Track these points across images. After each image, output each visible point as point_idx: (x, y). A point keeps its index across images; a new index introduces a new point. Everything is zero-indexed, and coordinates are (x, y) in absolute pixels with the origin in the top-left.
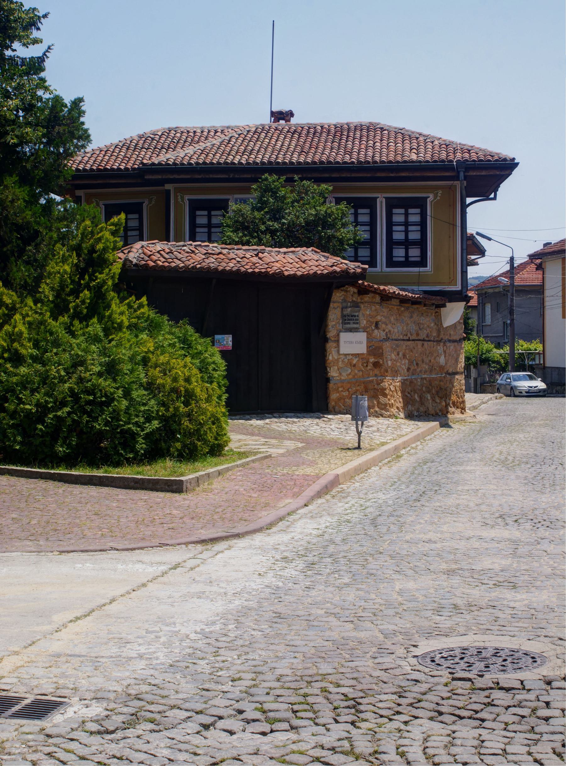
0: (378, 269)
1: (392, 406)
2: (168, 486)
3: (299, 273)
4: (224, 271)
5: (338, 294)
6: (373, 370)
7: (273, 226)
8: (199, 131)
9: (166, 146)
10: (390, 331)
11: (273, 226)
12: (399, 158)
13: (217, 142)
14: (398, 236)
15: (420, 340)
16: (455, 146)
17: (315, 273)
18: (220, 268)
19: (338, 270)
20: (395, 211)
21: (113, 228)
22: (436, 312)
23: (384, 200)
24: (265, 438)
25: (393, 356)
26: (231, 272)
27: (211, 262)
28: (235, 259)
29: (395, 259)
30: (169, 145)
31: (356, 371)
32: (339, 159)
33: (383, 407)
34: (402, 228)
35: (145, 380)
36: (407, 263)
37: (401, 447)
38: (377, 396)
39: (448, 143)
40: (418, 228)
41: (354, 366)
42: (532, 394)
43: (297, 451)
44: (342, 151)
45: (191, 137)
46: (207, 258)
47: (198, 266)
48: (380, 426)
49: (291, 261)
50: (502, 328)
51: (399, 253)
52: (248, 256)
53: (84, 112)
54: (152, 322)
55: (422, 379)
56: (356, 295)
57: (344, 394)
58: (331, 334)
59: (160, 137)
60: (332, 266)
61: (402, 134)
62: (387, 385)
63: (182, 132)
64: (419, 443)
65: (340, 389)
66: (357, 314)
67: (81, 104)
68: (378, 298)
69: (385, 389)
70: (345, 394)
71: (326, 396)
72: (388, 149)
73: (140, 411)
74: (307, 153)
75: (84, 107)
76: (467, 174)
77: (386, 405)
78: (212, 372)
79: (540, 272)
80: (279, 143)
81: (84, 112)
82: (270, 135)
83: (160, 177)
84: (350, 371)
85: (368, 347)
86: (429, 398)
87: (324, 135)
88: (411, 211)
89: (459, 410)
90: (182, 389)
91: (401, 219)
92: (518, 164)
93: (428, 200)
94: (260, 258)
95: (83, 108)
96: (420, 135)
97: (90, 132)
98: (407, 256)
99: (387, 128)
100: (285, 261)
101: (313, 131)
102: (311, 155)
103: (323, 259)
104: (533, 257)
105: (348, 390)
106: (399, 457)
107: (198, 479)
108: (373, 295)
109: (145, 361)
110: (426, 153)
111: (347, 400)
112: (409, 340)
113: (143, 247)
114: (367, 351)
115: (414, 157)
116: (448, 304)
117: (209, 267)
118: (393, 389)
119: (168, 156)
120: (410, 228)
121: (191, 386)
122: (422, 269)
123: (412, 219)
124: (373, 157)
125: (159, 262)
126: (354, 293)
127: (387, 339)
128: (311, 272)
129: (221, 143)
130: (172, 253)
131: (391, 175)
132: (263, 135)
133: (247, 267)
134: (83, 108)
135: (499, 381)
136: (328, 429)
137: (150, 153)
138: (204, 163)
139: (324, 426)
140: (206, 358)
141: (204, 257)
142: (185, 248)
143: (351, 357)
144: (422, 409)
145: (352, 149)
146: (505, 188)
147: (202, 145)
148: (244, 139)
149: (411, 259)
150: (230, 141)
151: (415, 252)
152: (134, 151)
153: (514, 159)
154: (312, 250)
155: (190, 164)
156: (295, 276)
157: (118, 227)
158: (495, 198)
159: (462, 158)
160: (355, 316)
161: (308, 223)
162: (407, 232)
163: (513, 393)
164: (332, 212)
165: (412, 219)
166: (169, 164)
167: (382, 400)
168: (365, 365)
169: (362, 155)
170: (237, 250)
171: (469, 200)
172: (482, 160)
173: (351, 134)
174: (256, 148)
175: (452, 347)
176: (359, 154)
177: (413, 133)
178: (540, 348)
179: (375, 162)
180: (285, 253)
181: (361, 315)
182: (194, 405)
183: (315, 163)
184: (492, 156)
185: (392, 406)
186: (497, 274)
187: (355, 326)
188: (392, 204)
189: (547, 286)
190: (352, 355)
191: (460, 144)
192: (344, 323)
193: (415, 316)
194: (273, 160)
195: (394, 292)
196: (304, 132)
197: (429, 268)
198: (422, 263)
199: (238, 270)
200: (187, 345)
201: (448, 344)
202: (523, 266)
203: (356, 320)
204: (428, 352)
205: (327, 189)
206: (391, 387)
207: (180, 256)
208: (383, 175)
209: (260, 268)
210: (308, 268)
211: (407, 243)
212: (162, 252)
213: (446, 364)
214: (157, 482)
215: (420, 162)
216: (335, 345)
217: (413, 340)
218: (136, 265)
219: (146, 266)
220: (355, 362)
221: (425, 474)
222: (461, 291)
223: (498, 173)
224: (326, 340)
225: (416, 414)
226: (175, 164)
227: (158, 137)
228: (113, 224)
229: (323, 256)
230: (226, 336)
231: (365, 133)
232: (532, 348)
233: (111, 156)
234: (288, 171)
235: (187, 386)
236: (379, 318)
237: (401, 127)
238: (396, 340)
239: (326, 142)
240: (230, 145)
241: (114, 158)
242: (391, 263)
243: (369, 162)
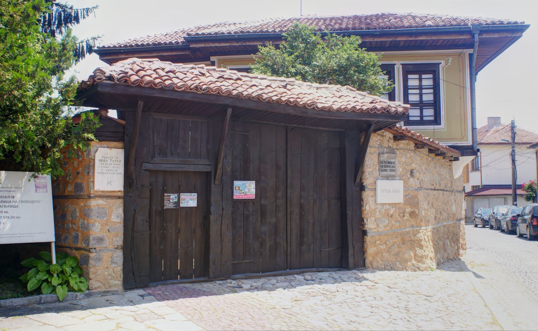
1: (426, 257)
5: (374, 138)
6: (410, 221)
7: (303, 68)
10: (422, 180)
15: (441, 190)
22: (450, 165)
23: (401, 66)
25: (426, 207)
27: (226, 86)
31: (393, 222)
33: (420, 259)
34: (417, 91)
38: (414, 247)
41: (392, 216)
52: (273, 86)
55: (444, 226)
56: (392, 141)
57: (382, 247)
58: (368, 181)
65: (378, 242)
66: (393, 161)
68: (412, 145)
69: (421, 240)
70: (383, 247)
76: (480, 37)
77: (422, 257)
84: (387, 222)
85: (405, 196)
91: (416, 83)
93: (440, 65)
98: (422, 116)
103: (360, 97)
105: (386, 243)
111: (384, 254)
112: (435, 190)
114: (404, 201)
116: (460, 158)
120: (424, 91)
123: (425, 83)
126: (390, 138)
127: (420, 188)
128: (349, 107)
131: (410, 39)
143: (388, 207)
144: (446, 256)
149: (425, 118)
153: (524, 22)
154: (347, 88)
160: (391, 163)
161: (340, 67)
162: (421, 95)
167: (419, 252)
168: (402, 215)
170: (261, 79)
181: (397, 162)
185: (426, 257)
187: (392, 173)
188: (408, 70)
190: (389, 204)
192: (381, 170)
198: (436, 121)
201: (457, 194)
203: (393, 167)
204: (446, 201)
206: (426, 237)
213: (456, 211)
216: (372, 193)
217: (437, 190)
220: (391, 212)
222: (472, 146)
223: (509, 35)
224: (362, 188)
229: (359, 94)
230: (248, 183)
236: (414, 166)
238: (427, 189)
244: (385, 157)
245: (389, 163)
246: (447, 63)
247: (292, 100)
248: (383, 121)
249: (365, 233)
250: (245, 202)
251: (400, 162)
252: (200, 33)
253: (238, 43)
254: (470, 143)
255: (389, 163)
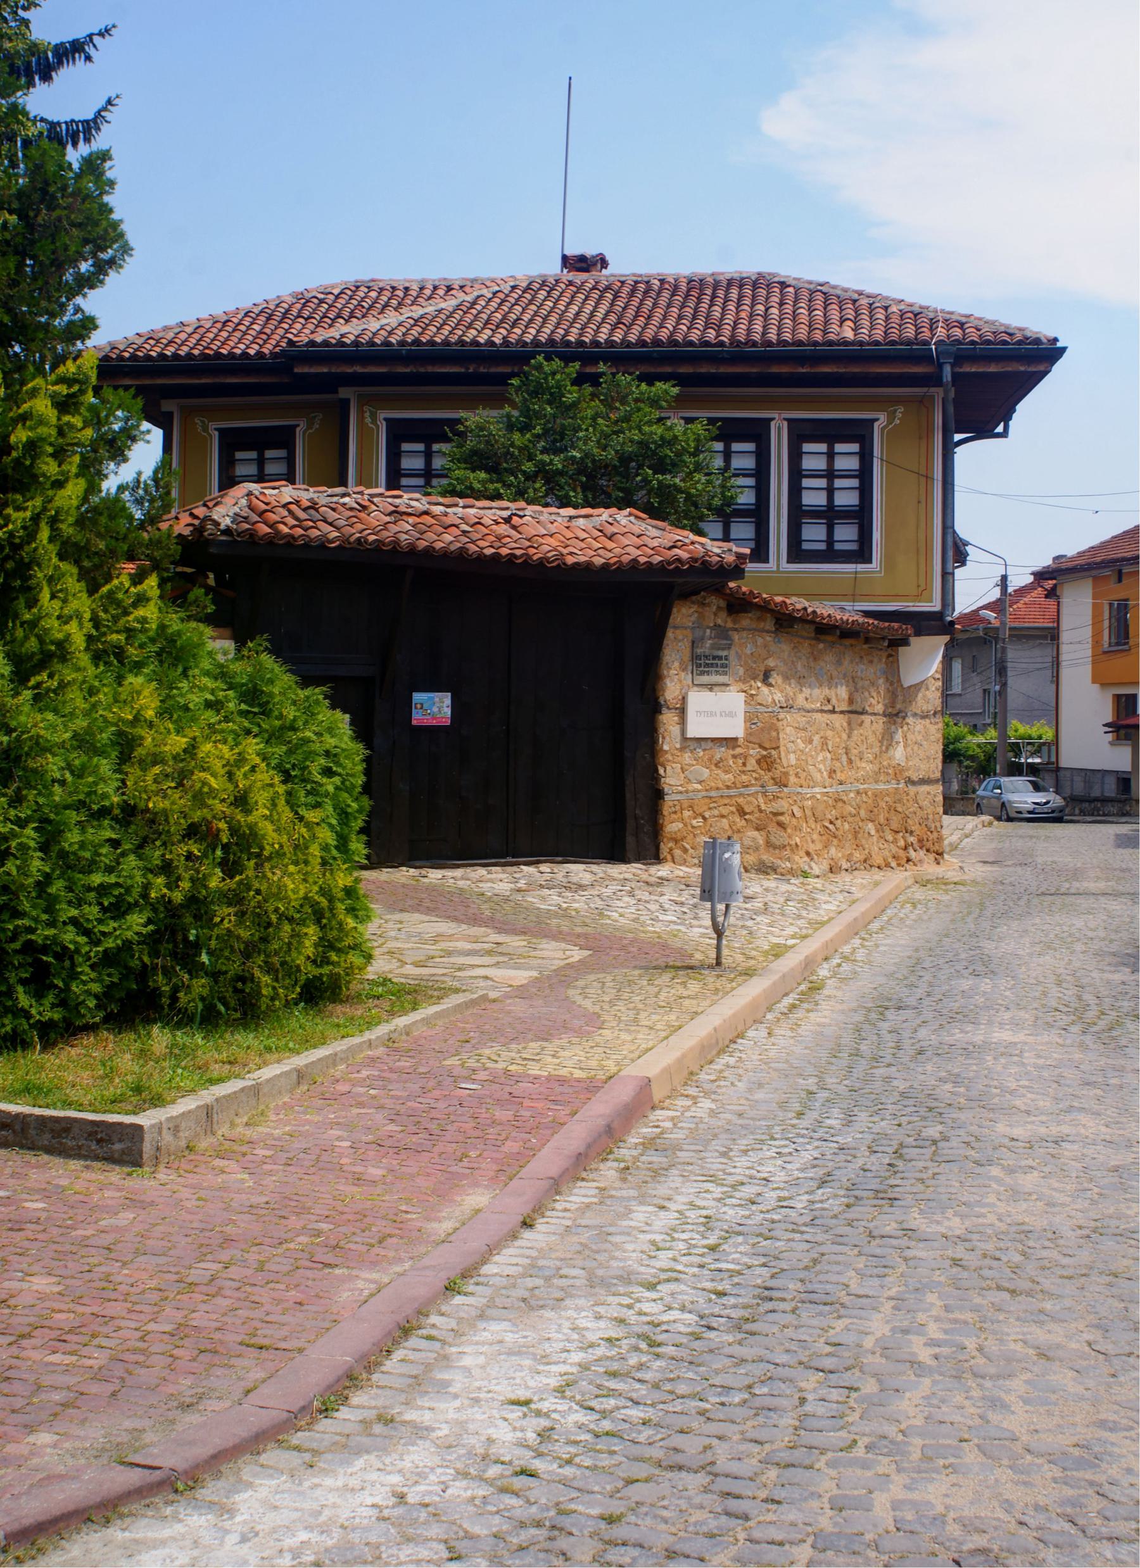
0: (772, 565)
2: (99, 1141)
3: (598, 561)
4: (429, 551)
5: (684, 610)
8: (415, 287)
9: (346, 314)
11: (551, 463)
12: (818, 336)
13: (450, 304)
14: (813, 498)
16: (931, 315)
17: (635, 560)
18: (422, 544)
19: (684, 555)
20: (807, 447)
21: (63, 389)
22: (890, 656)
24: (500, 931)
26: (445, 554)
27: (404, 532)
28: (457, 526)
29: (805, 546)
30: (352, 312)
32: (694, 336)
34: (822, 483)
35: (116, 799)
36: (830, 554)
37: (819, 958)
39: (916, 309)
40: (855, 483)
42: (1037, 817)
43: (565, 976)
44: (700, 322)
45: (399, 295)
46: (395, 523)
47: (372, 538)
48: (770, 897)
49: (583, 535)
50: (980, 700)
51: (814, 534)
52: (487, 521)
53: (112, 183)
54: (172, 641)
56: (723, 614)
59: (337, 297)
60: (670, 548)
61: (823, 295)
62: (786, 805)
63: (382, 289)
64: (857, 942)
66: (723, 653)
67: (108, 164)
68: (769, 624)
71: (656, 831)
72: (794, 320)
73: (89, 889)
74: (629, 327)
75: (111, 172)
76: (958, 370)
78: (318, 778)
79: (1052, 602)
80: (574, 309)
81: (112, 183)
82: (555, 294)
83: (326, 370)
86: (873, 832)
87: (666, 294)
88: (839, 447)
89: (932, 856)
90: (223, 825)
91: (820, 464)
92: (1063, 350)
93: (876, 425)
94: (514, 528)
95: (109, 174)
96: (860, 293)
97: (124, 227)
98: (830, 541)
99: (793, 283)
100: (569, 535)
101: (644, 289)
102: (636, 330)
104: (1040, 576)
106: (816, 988)
107: (208, 1111)
108: (758, 614)
109: (125, 747)
110: (872, 328)
112: (833, 712)
113: (250, 494)
115: (849, 334)
116: (913, 640)
117: (397, 542)
118: (798, 813)
119: (345, 329)
120: (838, 483)
121: (250, 819)
122: (861, 567)
123: (841, 464)
124: (764, 334)
125: (282, 527)
128: (626, 559)
129: (458, 307)
130: (317, 510)
132: (542, 294)
133: (482, 543)
134: (109, 174)
135: (980, 792)
136: (653, 907)
137: (311, 327)
138: (416, 342)
139: (645, 896)
140: (308, 741)
141: (388, 519)
142: (346, 500)
145: (722, 319)
146: (1030, 411)
147: (417, 312)
148: (503, 301)
149: (838, 546)
150: (474, 303)
151: (846, 533)
152: (280, 322)
153: (1056, 340)
154: (630, 514)
155: (387, 343)
156: (588, 567)
157: (76, 388)
158: (1004, 434)
159: (948, 337)
160: (720, 658)
162: (830, 491)
163: (1005, 814)
164: (676, 437)
165: (841, 464)
166: (344, 344)
169: (742, 329)
171: (958, 437)
172: (988, 342)
173: (721, 293)
174: (526, 317)
175: (918, 728)
176: (734, 328)
177: (846, 290)
178: (1048, 734)
179: (769, 343)
180: (571, 518)
181: (731, 658)
182: (250, 873)
183: (643, 344)
184: (1010, 335)
186: (974, 608)
188: (801, 433)
189: (1065, 624)
191: (942, 311)
193: (846, 663)
194: (558, 337)
195: (805, 609)
196: (626, 289)
197: (875, 565)
198: (862, 554)
199: (463, 550)
200: (260, 705)
202: (1022, 591)
205: (666, 392)
206: (796, 810)
207: (332, 515)
208: (785, 369)
209: (512, 545)
210: (618, 551)
211: (830, 515)
212: (293, 507)
214: (63, 1128)
215: (861, 343)
218: (227, 531)
219: (252, 534)
221: (889, 1059)
223: (1022, 369)
225: (845, 866)
226: (356, 343)
227: (332, 297)
228: (62, 380)
230: (436, 696)
231: (748, 291)
232: (1034, 735)
233: (234, 330)
234: (588, 360)
235: (240, 817)
236: (771, 663)
237: (822, 280)
239: (669, 306)
240: (474, 312)
241: (238, 334)
242: (797, 553)
243: (755, 344)
244: (706, 647)
245: (714, 658)
246: (891, 418)
247: (518, 552)
248: (704, 580)
249: (658, 795)
250: (432, 732)
251: (739, 657)
252: (319, 339)
253: (407, 366)
254: (935, 606)
255: (714, 658)
